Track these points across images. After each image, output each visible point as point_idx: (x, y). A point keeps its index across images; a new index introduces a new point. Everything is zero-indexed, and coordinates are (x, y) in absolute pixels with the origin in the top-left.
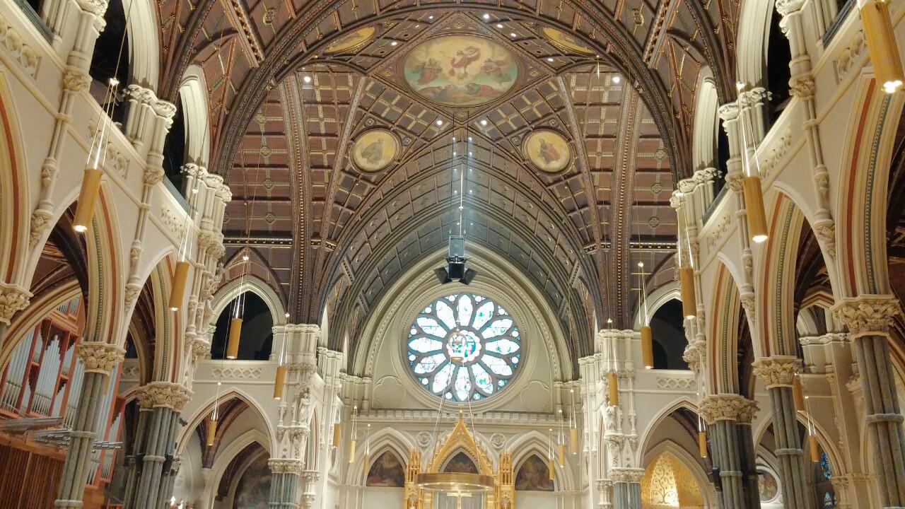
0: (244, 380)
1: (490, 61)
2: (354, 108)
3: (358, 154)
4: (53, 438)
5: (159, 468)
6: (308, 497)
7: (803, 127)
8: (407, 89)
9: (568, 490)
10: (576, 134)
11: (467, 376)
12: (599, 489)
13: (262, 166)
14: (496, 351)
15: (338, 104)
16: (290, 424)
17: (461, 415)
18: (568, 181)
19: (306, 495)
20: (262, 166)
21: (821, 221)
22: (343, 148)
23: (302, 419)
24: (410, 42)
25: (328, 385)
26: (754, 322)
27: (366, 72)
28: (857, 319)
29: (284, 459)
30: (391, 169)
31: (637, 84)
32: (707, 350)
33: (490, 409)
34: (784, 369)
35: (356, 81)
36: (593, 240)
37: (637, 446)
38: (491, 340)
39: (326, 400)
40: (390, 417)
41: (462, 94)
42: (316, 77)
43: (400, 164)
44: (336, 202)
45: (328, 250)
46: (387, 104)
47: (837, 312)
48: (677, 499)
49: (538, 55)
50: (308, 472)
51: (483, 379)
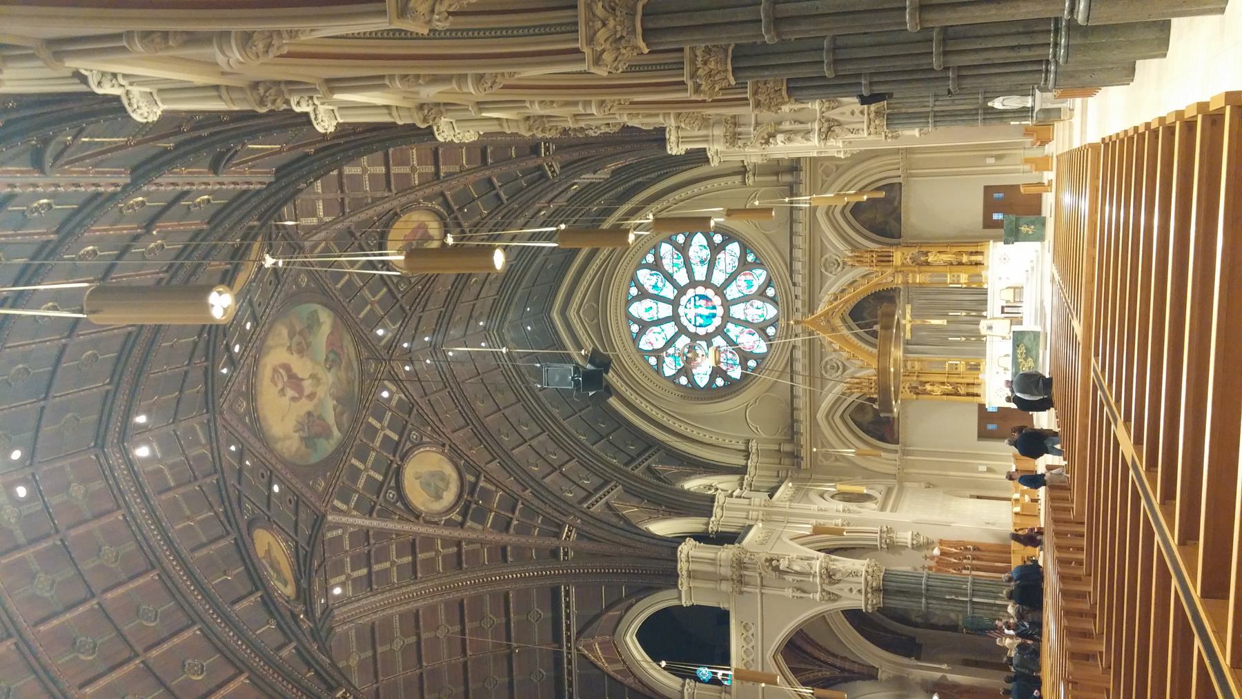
0: (757, 641)
1: (289, 349)
2: (374, 523)
3: (438, 506)
6: (915, 542)
8: (341, 449)
9: (899, 163)
10: (387, 206)
11: (742, 306)
12: (896, 137)
13: (463, 632)
14: (706, 266)
15: (369, 544)
16: (814, 584)
18: (456, 208)
19: (913, 544)
20: (463, 632)
22: (431, 530)
23: (808, 569)
24: (271, 468)
25: (761, 517)
27: (320, 515)
28: (619, 49)
29: (863, 592)
30: (454, 454)
31: (303, 185)
33: (788, 275)
35: (336, 526)
36: (540, 168)
38: (690, 273)
39: (780, 518)
40: (803, 415)
41: (342, 374)
42: (332, 581)
44: (507, 529)
45: (574, 535)
46: (369, 464)
49: (274, 281)
50: (881, 543)
51: (745, 284)
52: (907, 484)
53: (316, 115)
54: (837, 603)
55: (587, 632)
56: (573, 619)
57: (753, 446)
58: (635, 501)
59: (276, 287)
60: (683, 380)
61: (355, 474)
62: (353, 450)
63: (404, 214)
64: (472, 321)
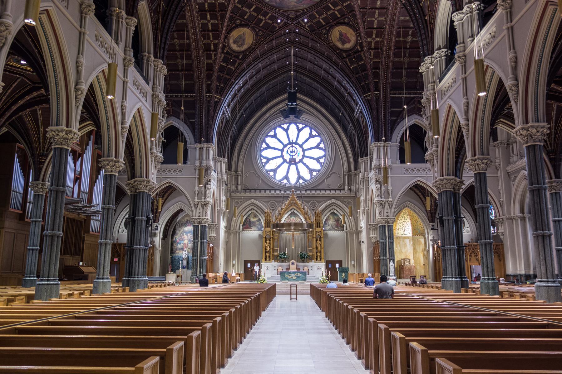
0: (174, 175)
4: (77, 209)
5: (144, 224)
7: (504, 28)
9: (352, 229)
17: (293, 191)
21: (511, 82)
26: (467, 138)
28: (527, 136)
30: (251, 50)
32: (439, 153)
34: (483, 163)
36: (369, 91)
37: (392, 206)
40: (253, 194)
43: (256, 47)
45: (216, 100)
47: (517, 132)
48: (411, 232)
53: (461, 13)
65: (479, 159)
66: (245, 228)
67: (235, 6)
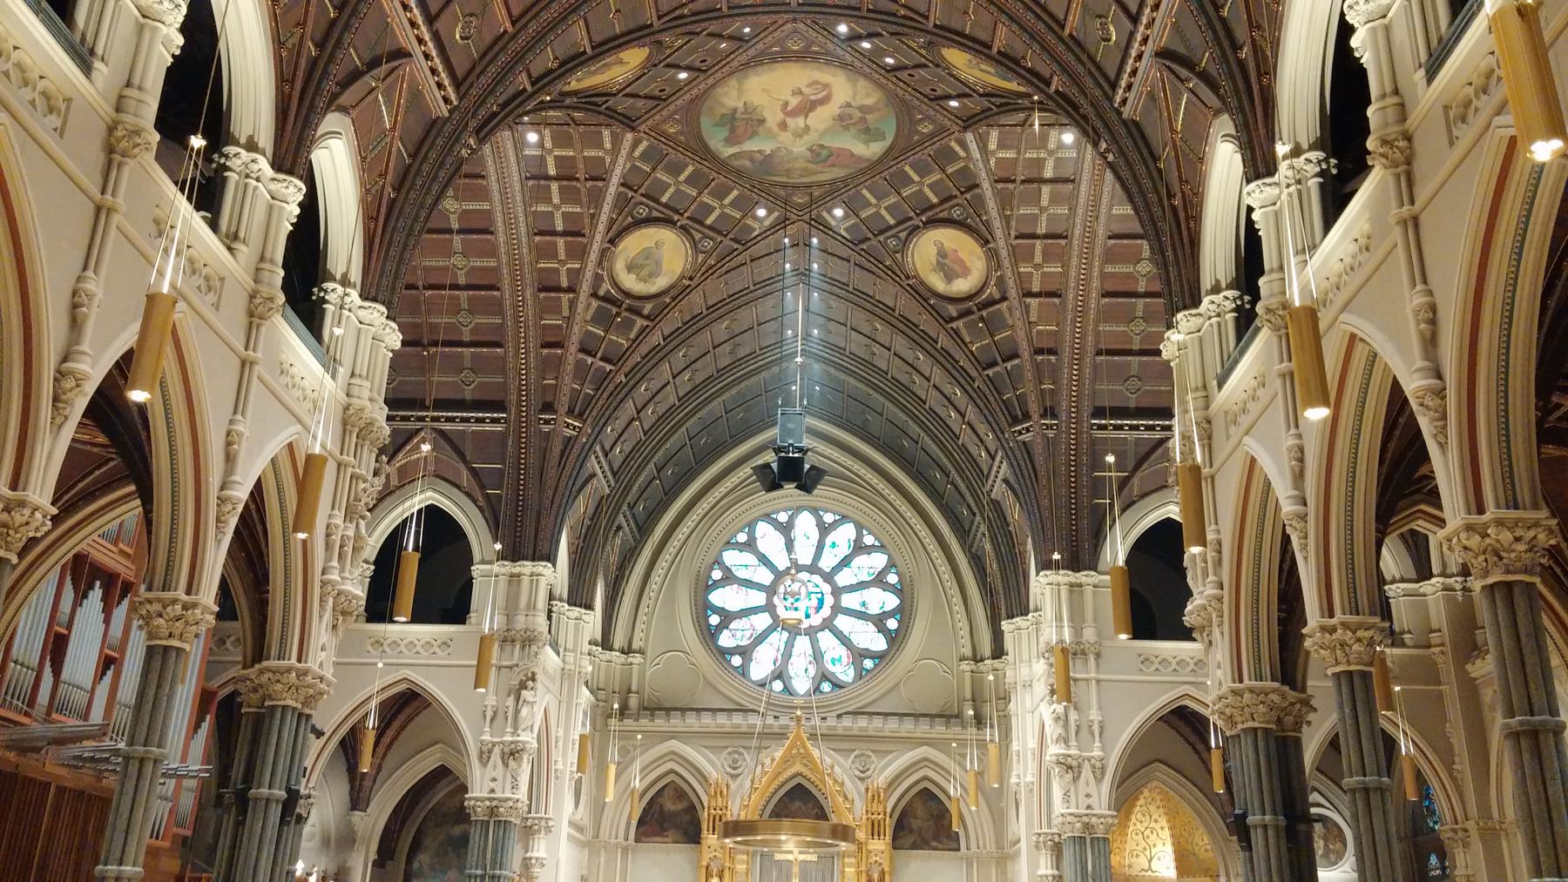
0: (423, 658)
1: (848, 105)
2: (613, 188)
3: (620, 266)
4: (92, 759)
5: (275, 812)
6: (533, 861)
7: (1392, 221)
9: (985, 848)
10: (999, 233)
12: (1037, 847)
13: (455, 287)
14: (859, 609)
15: (586, 179)
17: (799, 719)
18: (984, 313)
19: (530, 859)
22: (594, 256)
25: (567, 667)
26: (1306, 558)
28: (1484, 553)
30: (677, 292)
32: (1226, 607)
33: (850, 709)
34: (1359, 640)
36: (1027, 416)
37: (1103, 774)
38: (852, 588)
40: (676, 722)
41: (801, 164)
42: (547, 132)
43: (693, 284)
44: (583, 350)
45: (569, 432)
46: (683, 188)
47: (1450, 540)
48: (1172, 865)
50: (534, 819)
52: (586, 852)
54: (476, 761)
55: (442, 442)
56: (460, 427)
57: (636, 659)
58: (590, 511)
59: (926, 96)
60: (717, 574)
61: (675, 170)
62: (705, 169)
63: (986, 253)
64: (822, 321)
65: (1345, 625)
66: (646, 834)
67: (634, 167)
